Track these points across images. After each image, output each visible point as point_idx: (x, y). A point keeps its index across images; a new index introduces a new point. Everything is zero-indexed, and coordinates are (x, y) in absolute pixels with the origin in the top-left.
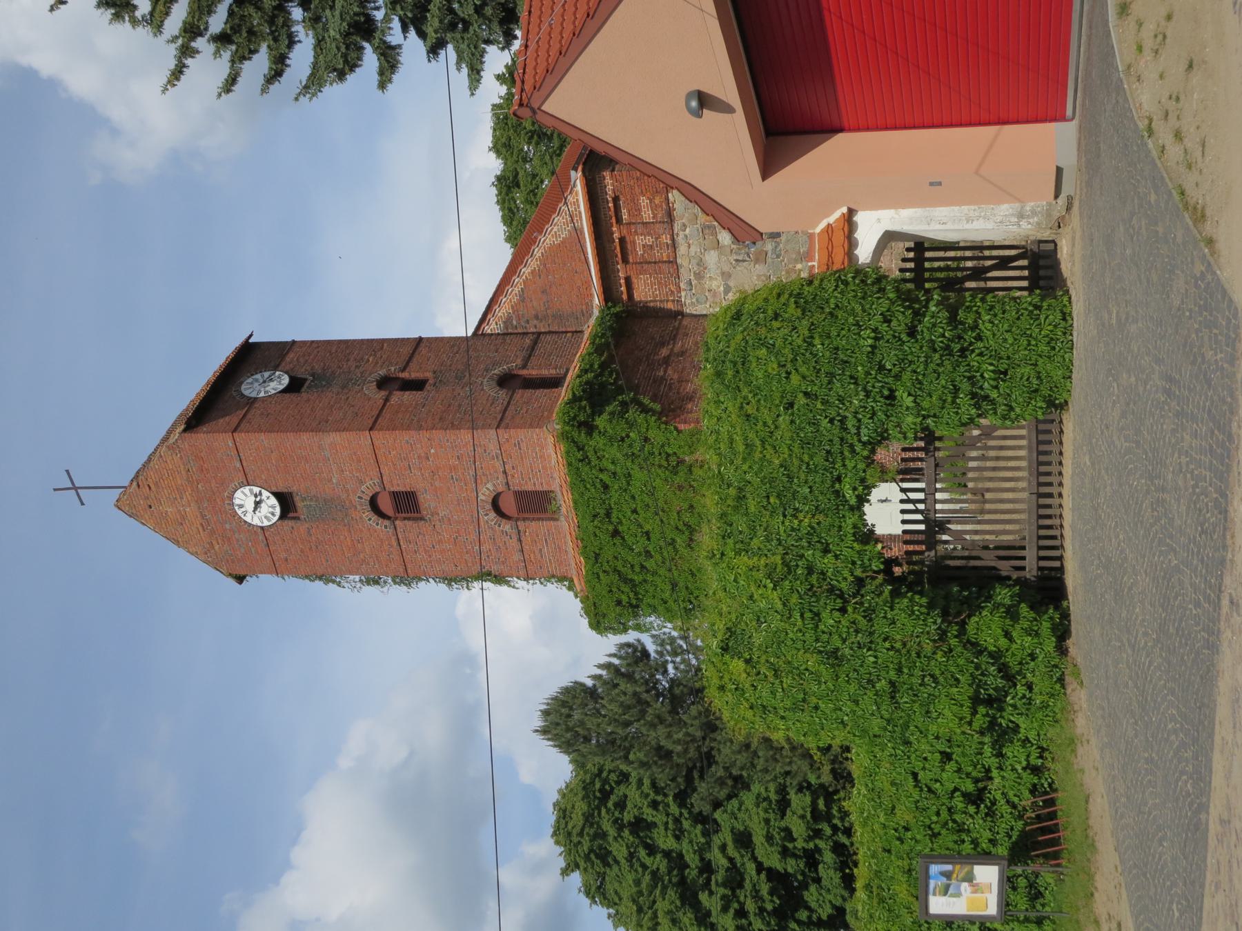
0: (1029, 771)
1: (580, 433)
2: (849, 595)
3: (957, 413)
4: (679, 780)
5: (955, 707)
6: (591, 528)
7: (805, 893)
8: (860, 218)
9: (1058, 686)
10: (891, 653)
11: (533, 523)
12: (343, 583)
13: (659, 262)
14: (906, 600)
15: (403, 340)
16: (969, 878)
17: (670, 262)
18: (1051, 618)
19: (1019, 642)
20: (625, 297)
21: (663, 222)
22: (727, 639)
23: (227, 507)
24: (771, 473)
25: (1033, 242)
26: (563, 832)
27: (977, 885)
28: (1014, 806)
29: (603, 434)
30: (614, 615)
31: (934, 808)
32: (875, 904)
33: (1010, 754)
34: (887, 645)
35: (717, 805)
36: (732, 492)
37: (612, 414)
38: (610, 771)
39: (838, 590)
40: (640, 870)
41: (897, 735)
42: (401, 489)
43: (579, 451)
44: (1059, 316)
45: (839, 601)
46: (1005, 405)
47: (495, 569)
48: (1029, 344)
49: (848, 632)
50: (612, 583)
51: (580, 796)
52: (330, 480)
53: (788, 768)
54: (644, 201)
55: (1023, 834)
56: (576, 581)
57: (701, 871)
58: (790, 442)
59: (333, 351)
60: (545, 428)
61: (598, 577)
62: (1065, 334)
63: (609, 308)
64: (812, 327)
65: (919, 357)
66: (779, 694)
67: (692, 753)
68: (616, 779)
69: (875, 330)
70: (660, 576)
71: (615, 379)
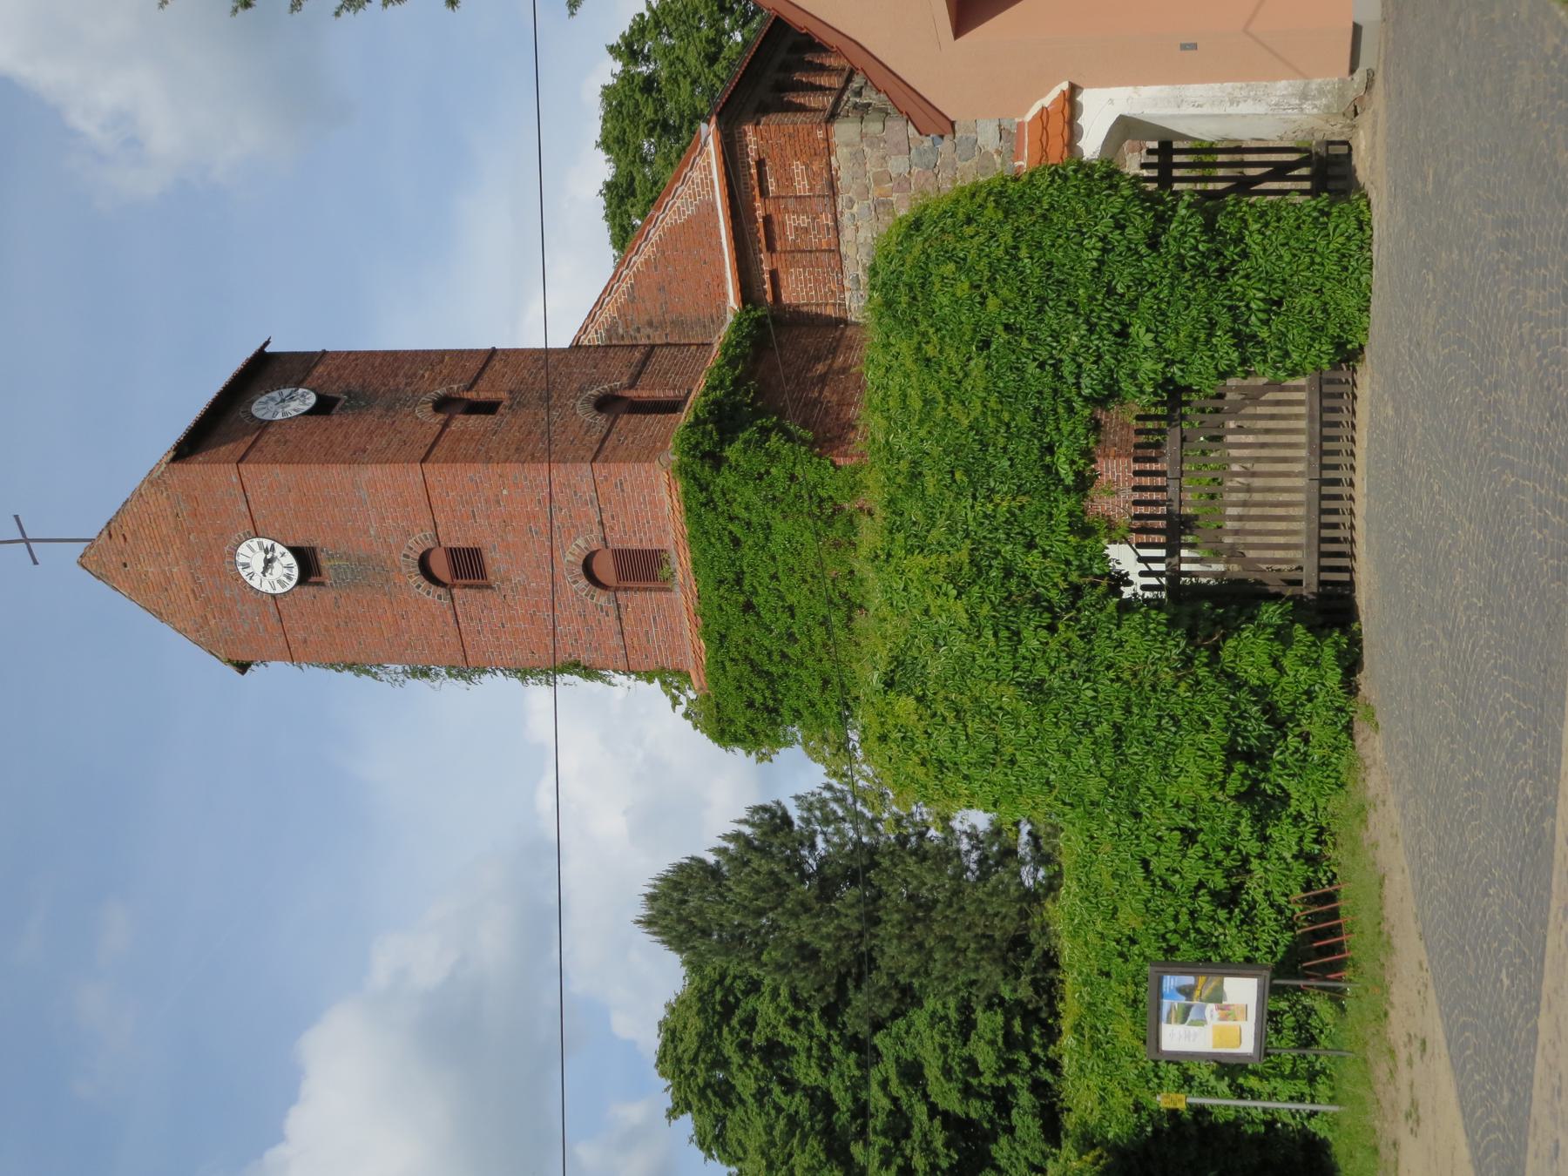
0: (1302, 861)
1: (703, 466)
2: (1060, 607)
3: (1212, 357)
4: (828, 989)
5: (1202, 760)
6: (715, 600)
7: (993, 1147)
8: (1086, 98)
9: (1343, 737)
10: (1117, 685)
11: (638, 595)
12: (381, 675)
13: (817, 250)
14: (1137, 617)
15: (471, 351)
16: (1217, 997)
17: (830, 251)
18: (1336, 643)
19: (1292, 673)
20: (769, 298)
21: (823, 196)
22: (892, 671)
23: (229, 567)
24: (958, 438)
25: (1319, 144)
26: (671, 1058)
27: (1227, 1007)
28: (1280, 911)
29: (735, 468)
30: (743, 721)
31: (1171, 910)
32: (1087, 1052)
33: (1276, 835)
34: (1111, 674)
35: (878, 1026)
36: (904, 466)
37: (747, 442)
38: (735, 977)
39: (1046, 600)
40: (773, 1113)
41: (1121, 804)
42: (461, 544)
43: (701, 491)
44: (1354, 224)
45: (1046, 615)
46: (1278, 348)
47: (585, 658)
48: (1313, 263)
49: (1058, 658)
50: (742, 675)
51: (695, 1009)
52: (367, 532)
53: (973, 977)
54: (798, 167)
55: (1290, 950)
56: (693, 676)
57: (854, 1117)
58: (984, 395)
59: (377, 364)
60: (657, 462)
61: (724, 668)
62: (1361, 248)
63: (748, 312)
64: (1018, 233)
65: (1163, 278)
66: (962, 743)
67: (846, 953)
68: (743, 988)
69: (1103, 239)
70: (807, 668)
71: (753, 399)
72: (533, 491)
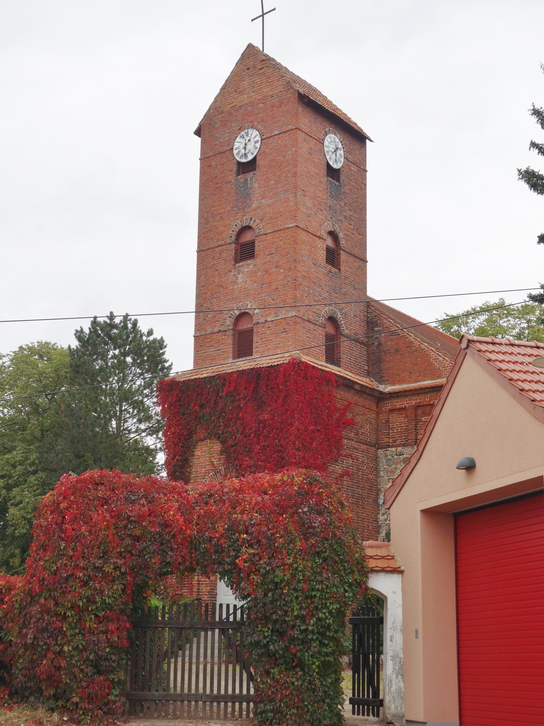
42: (256, 248)
72: (282, 285)
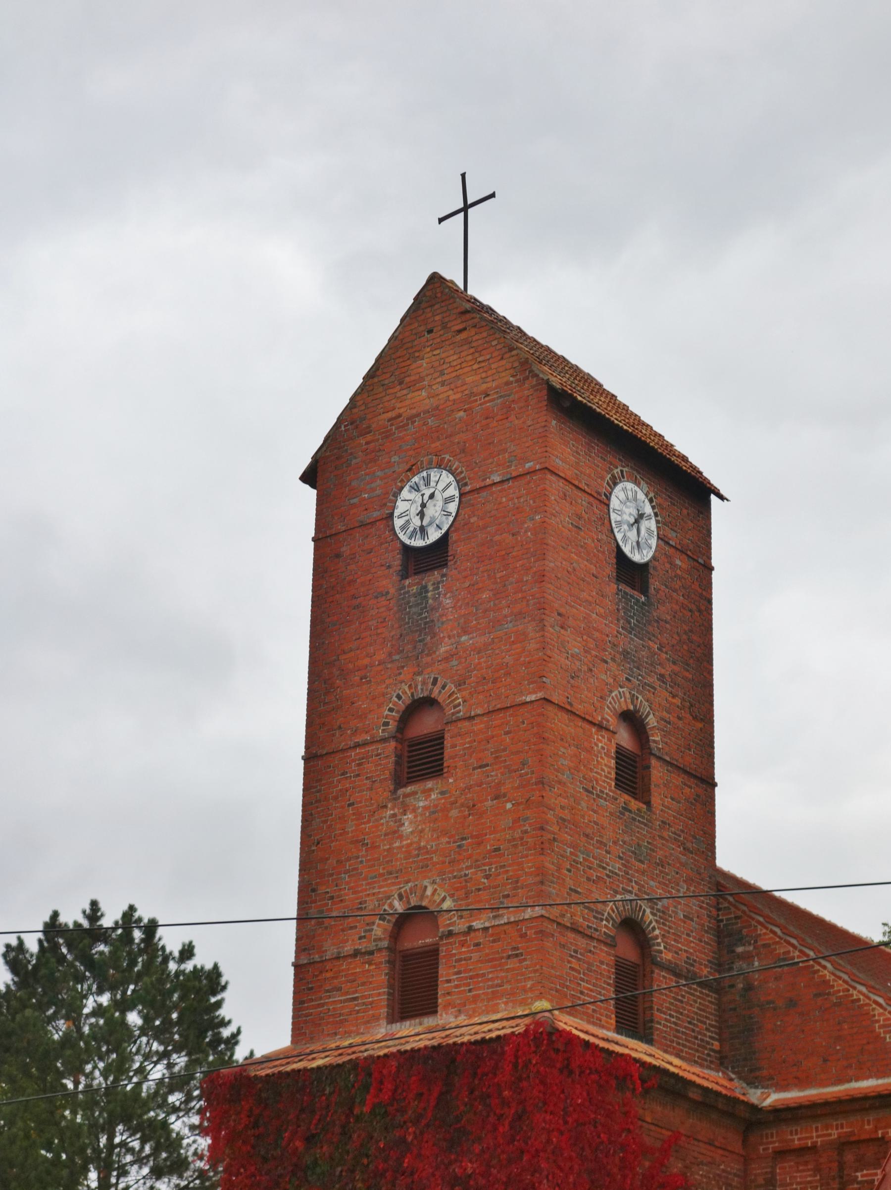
42: (448, 751)
72: (509, 841)
